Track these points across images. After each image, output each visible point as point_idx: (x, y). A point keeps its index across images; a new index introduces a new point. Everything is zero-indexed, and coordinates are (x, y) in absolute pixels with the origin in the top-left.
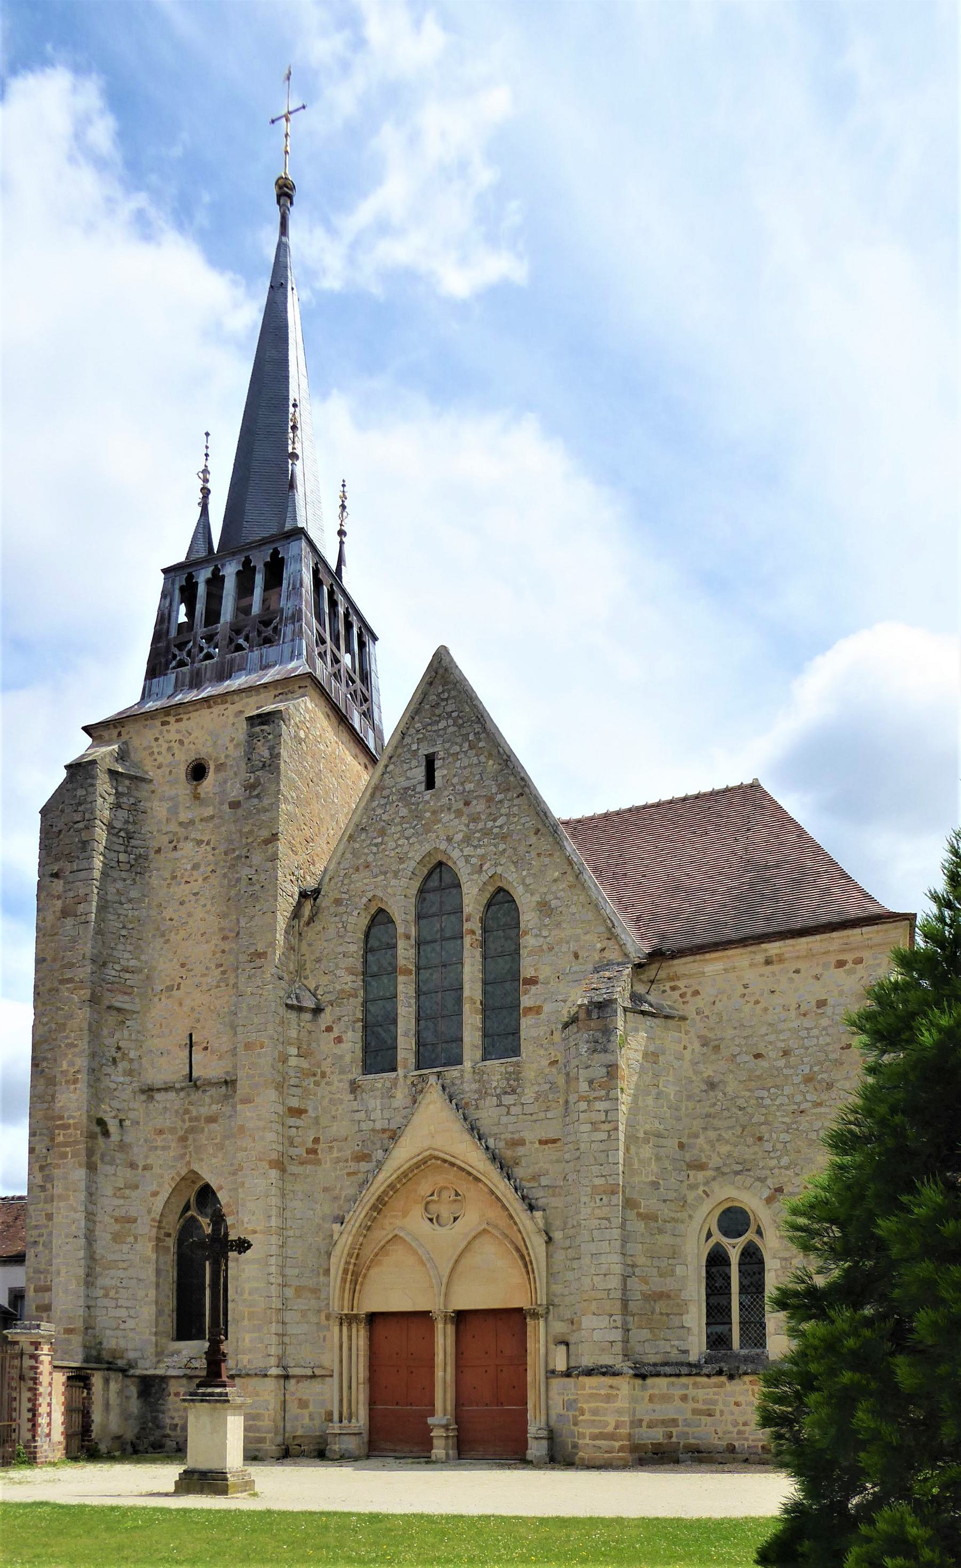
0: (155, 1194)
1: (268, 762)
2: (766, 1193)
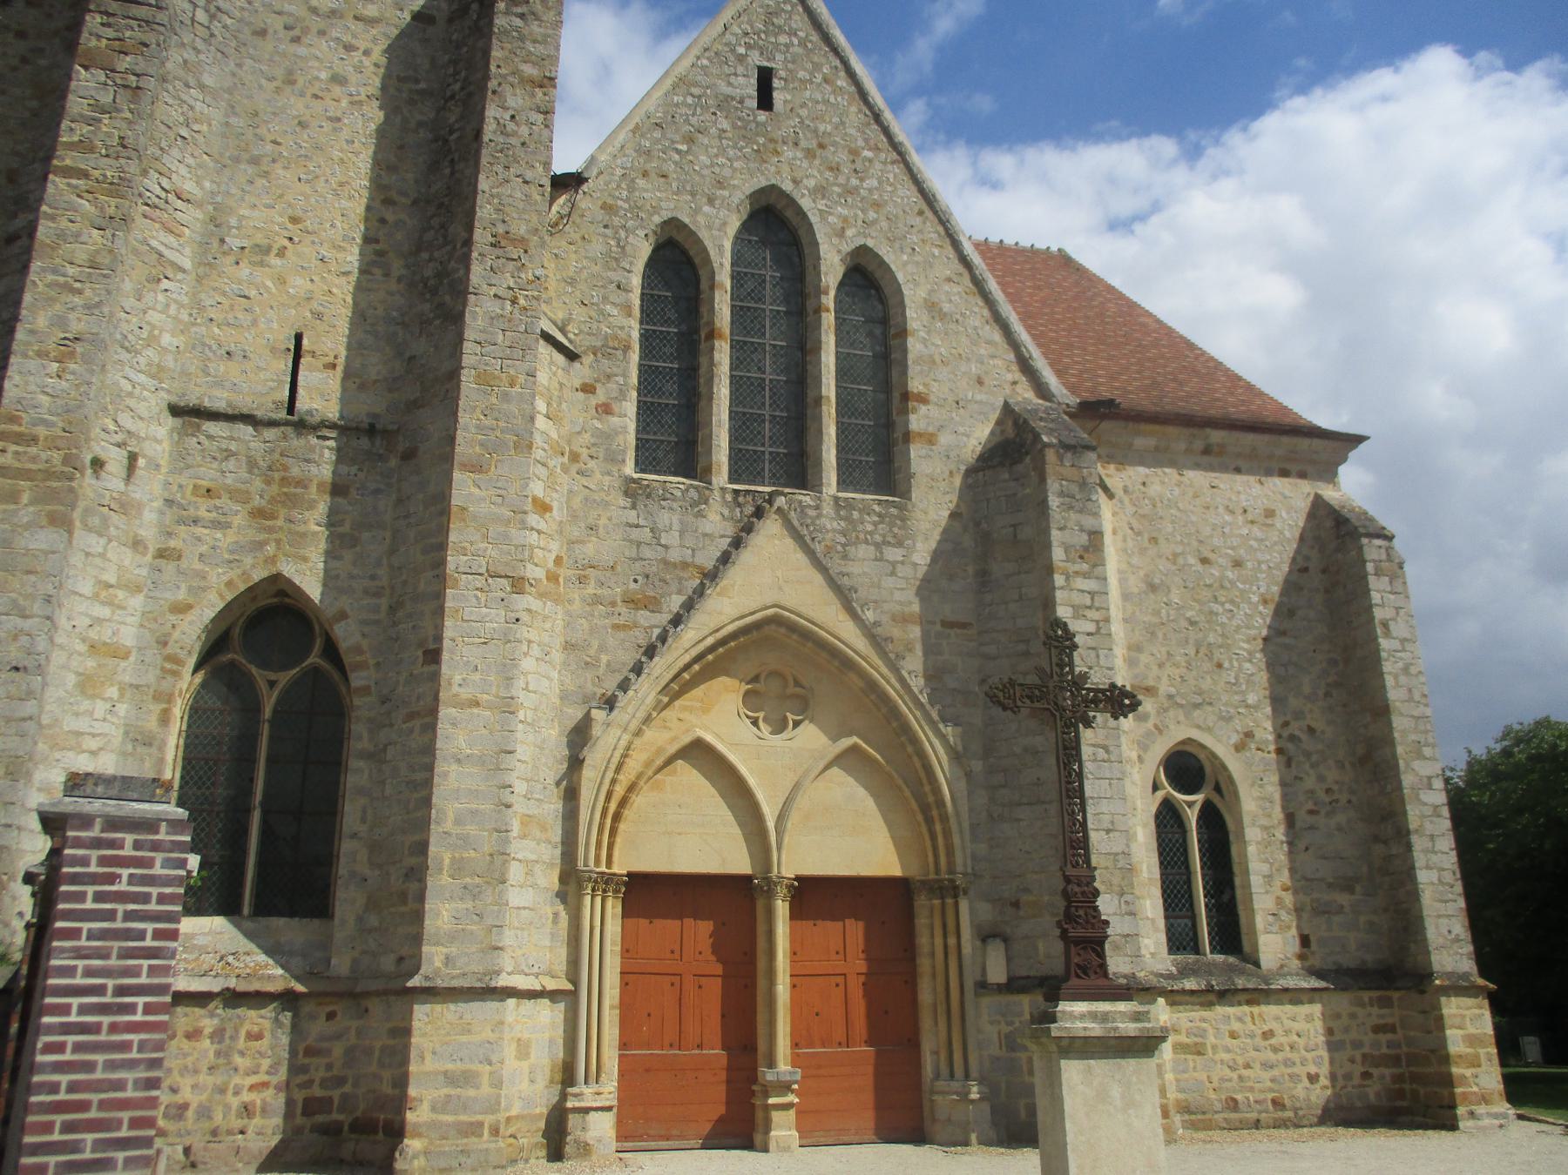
0: (181, 609)
2: (1235, 738)
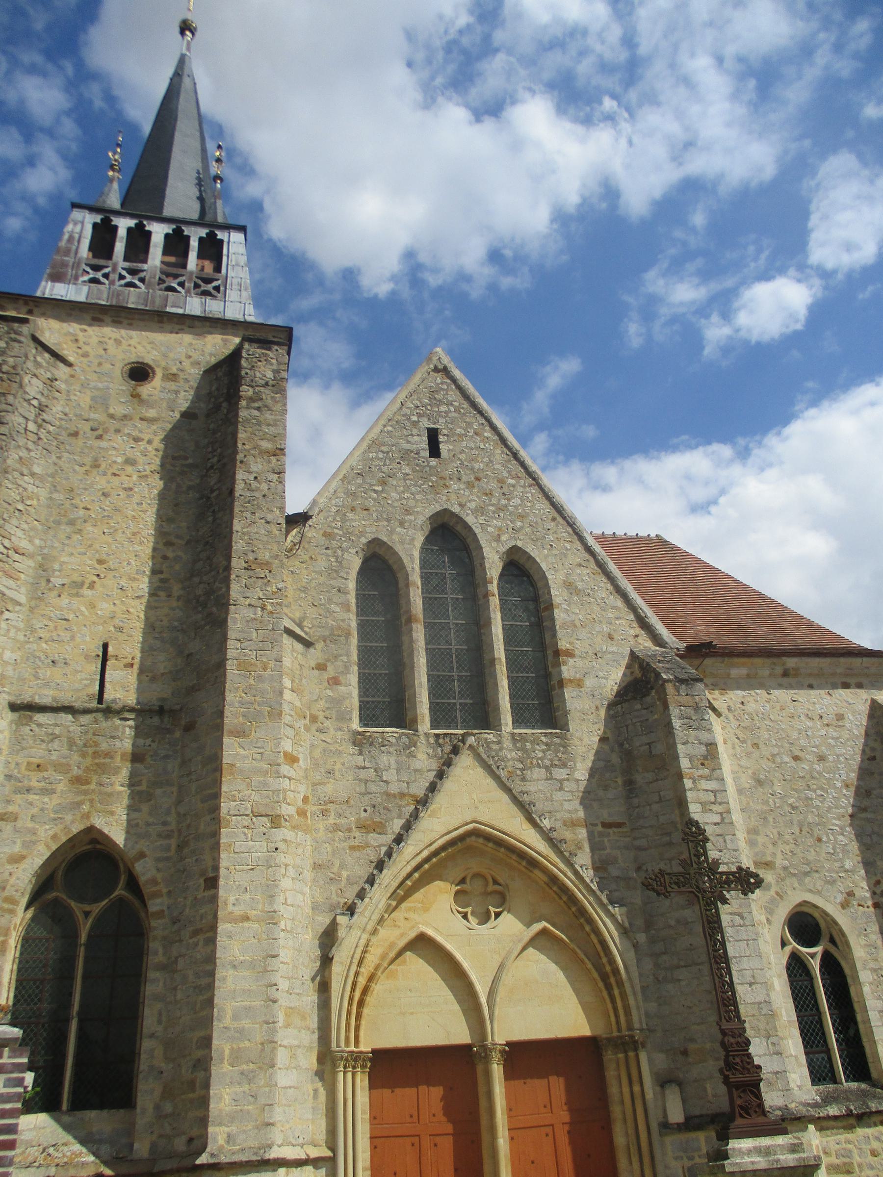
0: (17, 859)
1: (271, 383)
